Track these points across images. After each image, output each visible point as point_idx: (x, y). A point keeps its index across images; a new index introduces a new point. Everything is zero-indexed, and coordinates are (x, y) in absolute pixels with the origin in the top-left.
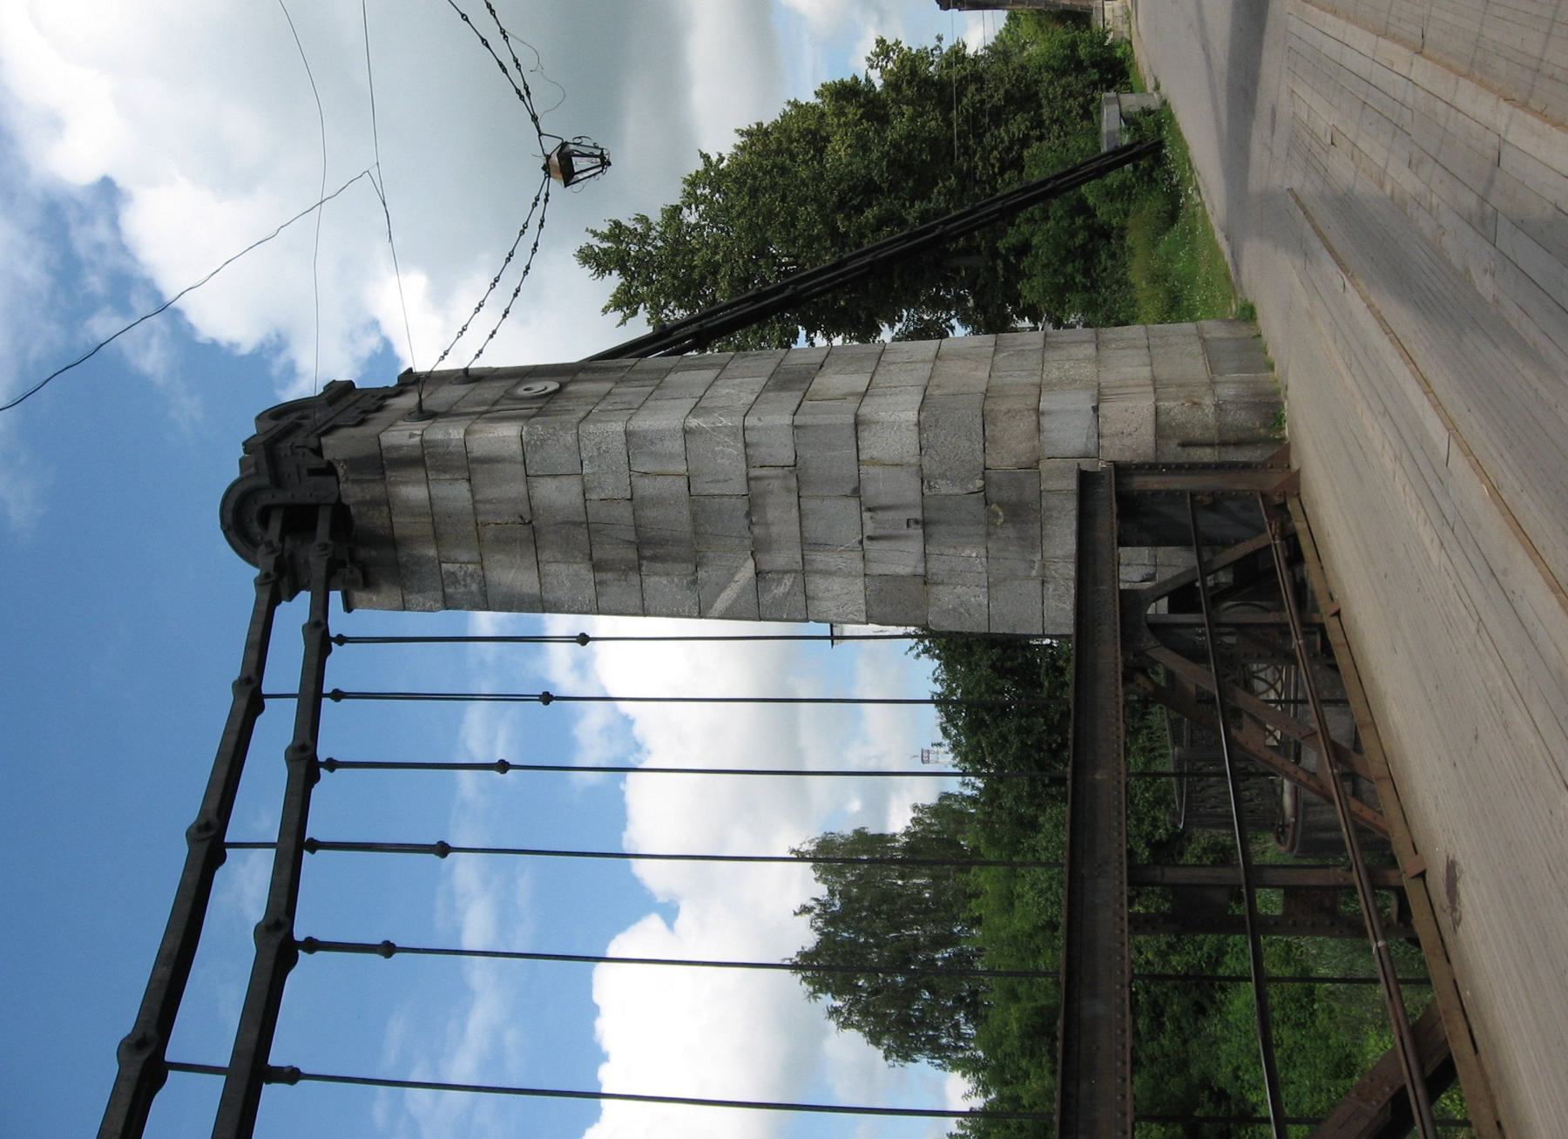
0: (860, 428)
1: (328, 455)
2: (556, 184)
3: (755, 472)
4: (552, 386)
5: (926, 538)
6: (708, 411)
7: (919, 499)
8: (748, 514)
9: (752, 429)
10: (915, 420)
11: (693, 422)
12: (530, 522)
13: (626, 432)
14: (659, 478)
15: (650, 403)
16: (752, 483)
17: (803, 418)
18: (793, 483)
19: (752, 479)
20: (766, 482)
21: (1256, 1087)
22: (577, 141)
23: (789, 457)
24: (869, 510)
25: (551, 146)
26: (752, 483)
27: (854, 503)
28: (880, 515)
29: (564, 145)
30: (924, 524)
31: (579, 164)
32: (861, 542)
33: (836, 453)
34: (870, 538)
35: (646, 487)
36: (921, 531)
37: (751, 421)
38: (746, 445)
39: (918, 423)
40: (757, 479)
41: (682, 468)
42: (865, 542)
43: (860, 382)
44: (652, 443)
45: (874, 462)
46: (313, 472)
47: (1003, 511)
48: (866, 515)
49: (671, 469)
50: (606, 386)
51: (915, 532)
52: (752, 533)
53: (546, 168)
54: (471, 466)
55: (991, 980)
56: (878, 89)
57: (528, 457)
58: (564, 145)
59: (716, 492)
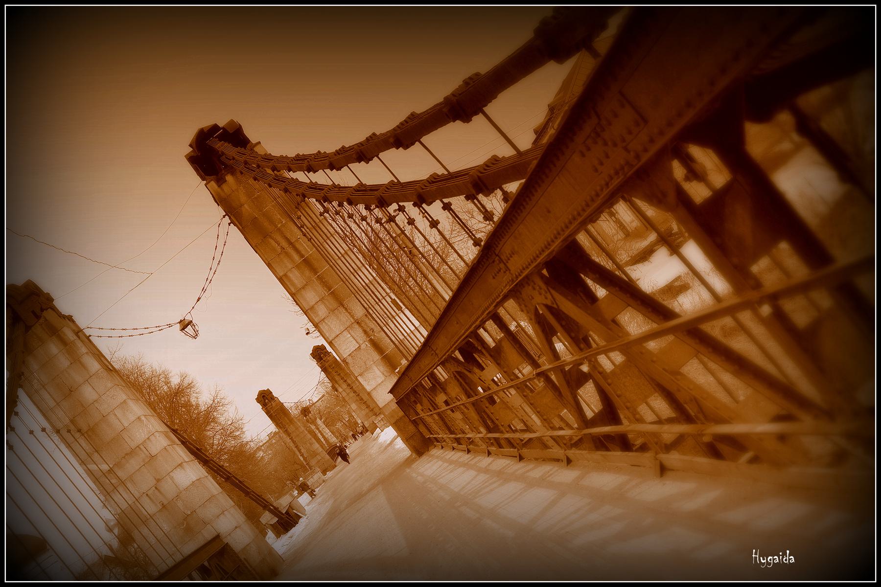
0: (179, 467)
1: (45, 313)
2: (178, 326)
3: (142, 447)
4: (112, 369)
5: (160, 511)
6: (145, 417)
7: (171, 499)
8: (127, 454)
9: (155, 437)
10: (194, 481)
11: (143, 418)
12: (72, 391)
13: (125, 401)
14: (117, 420)
15: (133, 401)
16: (138, 448)
17: (169, 448)
18: (147, 461)
19: (139, 447)
20: (141, 452)
21: (390, 268)
22: (195, 325)
23: (154, 453)
24: (156, 488)
25: (188, 318)
26: (138, 448)
27: (154, 482)
28: (156, 491)
29: (191, 321)
30: (164, 506)
31: (189, 329)
32: (144, 493)
33: (166, 465)
34: (147, 495)
35: (112, 418)
36: (161, 507)
37: (157, 434)
38: (148, 438)
39: (193, 482)
40: (140, 448)
41: (126, 425)
42: (145, 494)
43: (187, 460)
44: (127, 411)
45: (172, 478)
46: (34, 313)
47: (186, 526)
48: (154, 488)
49: (123, 421)
50: (124, 385)
51: (160, 506)
52: (121, 459)
53: (181, 321)
54: (77, 361)
55: (488, 216)
56: (633, 198)
57: (94, 377)
58: (191, 321)
59: (126, 440)
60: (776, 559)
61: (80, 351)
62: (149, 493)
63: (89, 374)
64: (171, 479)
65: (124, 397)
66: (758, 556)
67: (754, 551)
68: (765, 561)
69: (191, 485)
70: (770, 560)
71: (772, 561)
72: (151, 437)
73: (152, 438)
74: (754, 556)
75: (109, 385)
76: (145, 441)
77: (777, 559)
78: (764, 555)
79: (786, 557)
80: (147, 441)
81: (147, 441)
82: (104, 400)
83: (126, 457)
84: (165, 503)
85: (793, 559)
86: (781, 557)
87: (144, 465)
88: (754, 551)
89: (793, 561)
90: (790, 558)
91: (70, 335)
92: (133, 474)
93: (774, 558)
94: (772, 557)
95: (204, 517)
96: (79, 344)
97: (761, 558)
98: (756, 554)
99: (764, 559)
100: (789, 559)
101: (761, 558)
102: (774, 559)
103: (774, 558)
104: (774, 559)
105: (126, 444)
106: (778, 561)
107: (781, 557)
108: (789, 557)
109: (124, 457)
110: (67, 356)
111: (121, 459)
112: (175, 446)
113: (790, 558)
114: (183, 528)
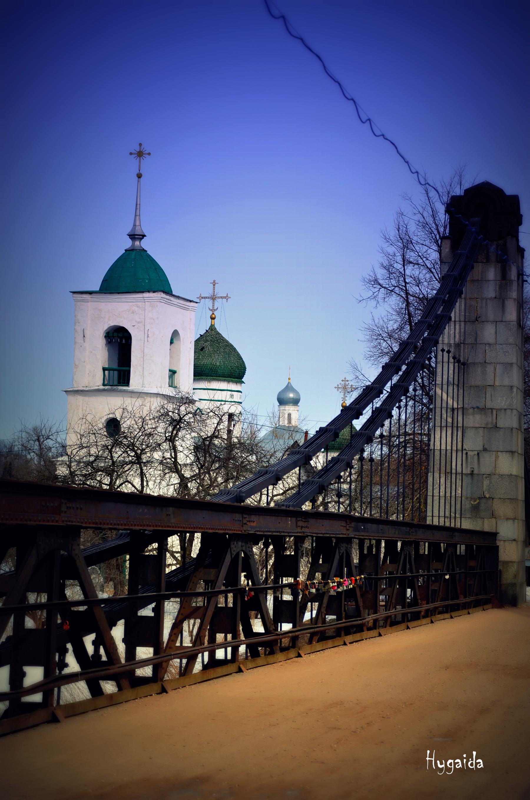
0: (510, 453)
3: (494, 412)
7: (482, 473)
8: (478, 408)
9: (512, 412)
10: (512, 474)
11: (515, 390)
13: (512, 364)
14: (493, 374)
16: (490, 410)
20: (490, 416)
24: (478, 454)
28: (476, 457)
36: (469, 473)
37: (515, 412)
38: (505, 410)
39: (511, 475)
40: (492, 412)
41: (497, 383)
45: (497, 457)
48: (476, 453)
49: (497, 379)
52: (470, 408)
57: (504, 323)
60: (458, 763)
61: (511, 293)
62: (470, 453)
63: (502, 318)
64: (496, 457)
65: (514, 360)
66: (433, 759)
67: (428, 752)
68: (443, 766)
69: (508, 475)
70: (451, 764)
71: (453, 766)
72: (508, 410)
73: (509, 412)
74: (428, 759)
75: (511, 340)
76: (501, 409)
77: (460, 763)
78: (443, 758)
79: (472, 760)
80: (503, 411)
81: (503, 411)
82: (496, 349)
83: (476, 409)
84: (476, 472)
85: (482, 764)
86: (465, 760)
87: (484, 428)
88: (428, 752)
89: (482, 766)
90: (478, 761)
91: (513, 274)
92: (470, 427)
93: (456, 761)
94: (452, 761)
95: (496, 509)
96: (515, 286)
97: (438, 762)
98: (431, 756)
99: (441, 764)
100: (477, 764)
101: (438, 762)
102: (455, 764)
103: (456, 761)
104: (455, 764)
105: (484, 399)
106: (461, 766)
107: (465, 760)
108: (476, 760)
109: (474, 408)
110: (497, 289)
111: (470, 408)
112: (519, 432)
113: (478, 761)
114: (472, 503)
